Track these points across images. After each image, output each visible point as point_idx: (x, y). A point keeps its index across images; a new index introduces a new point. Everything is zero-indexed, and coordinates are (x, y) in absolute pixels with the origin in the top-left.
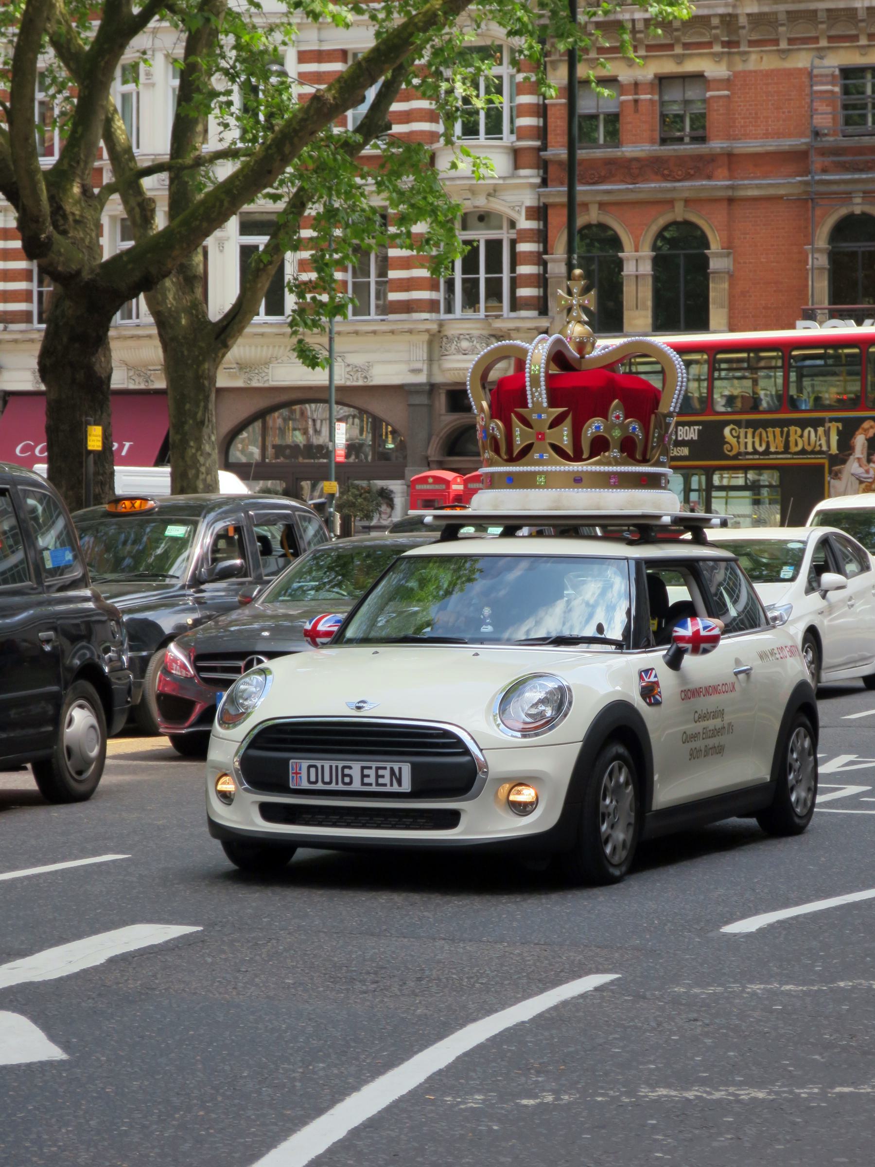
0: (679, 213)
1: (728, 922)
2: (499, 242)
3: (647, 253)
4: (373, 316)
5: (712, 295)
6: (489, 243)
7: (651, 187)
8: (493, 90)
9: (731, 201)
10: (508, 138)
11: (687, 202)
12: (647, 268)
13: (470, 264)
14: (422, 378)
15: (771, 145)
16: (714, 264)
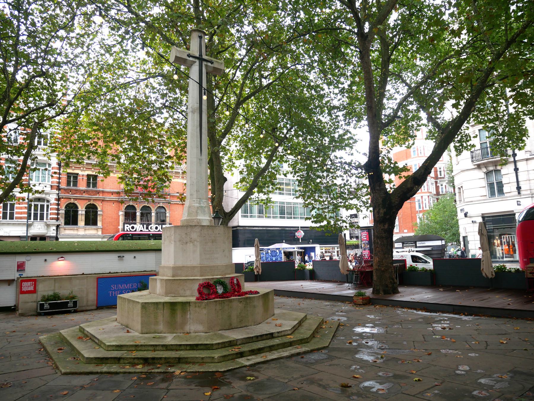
0: (92, 202)
1: (359, 325)
2: (44, 205)
3: (84, 209)
4: (14, 220)
5: (98, 219)
6: (41, 205)
7: (85, 196)
8: (494, 88)
9: (103, 200)
10: (351, 128)
11: (94, 200)
12: (84, 213)
13: (36, 210)
14: (25, 235)
15: (112, 190)
16: (99, 213)
